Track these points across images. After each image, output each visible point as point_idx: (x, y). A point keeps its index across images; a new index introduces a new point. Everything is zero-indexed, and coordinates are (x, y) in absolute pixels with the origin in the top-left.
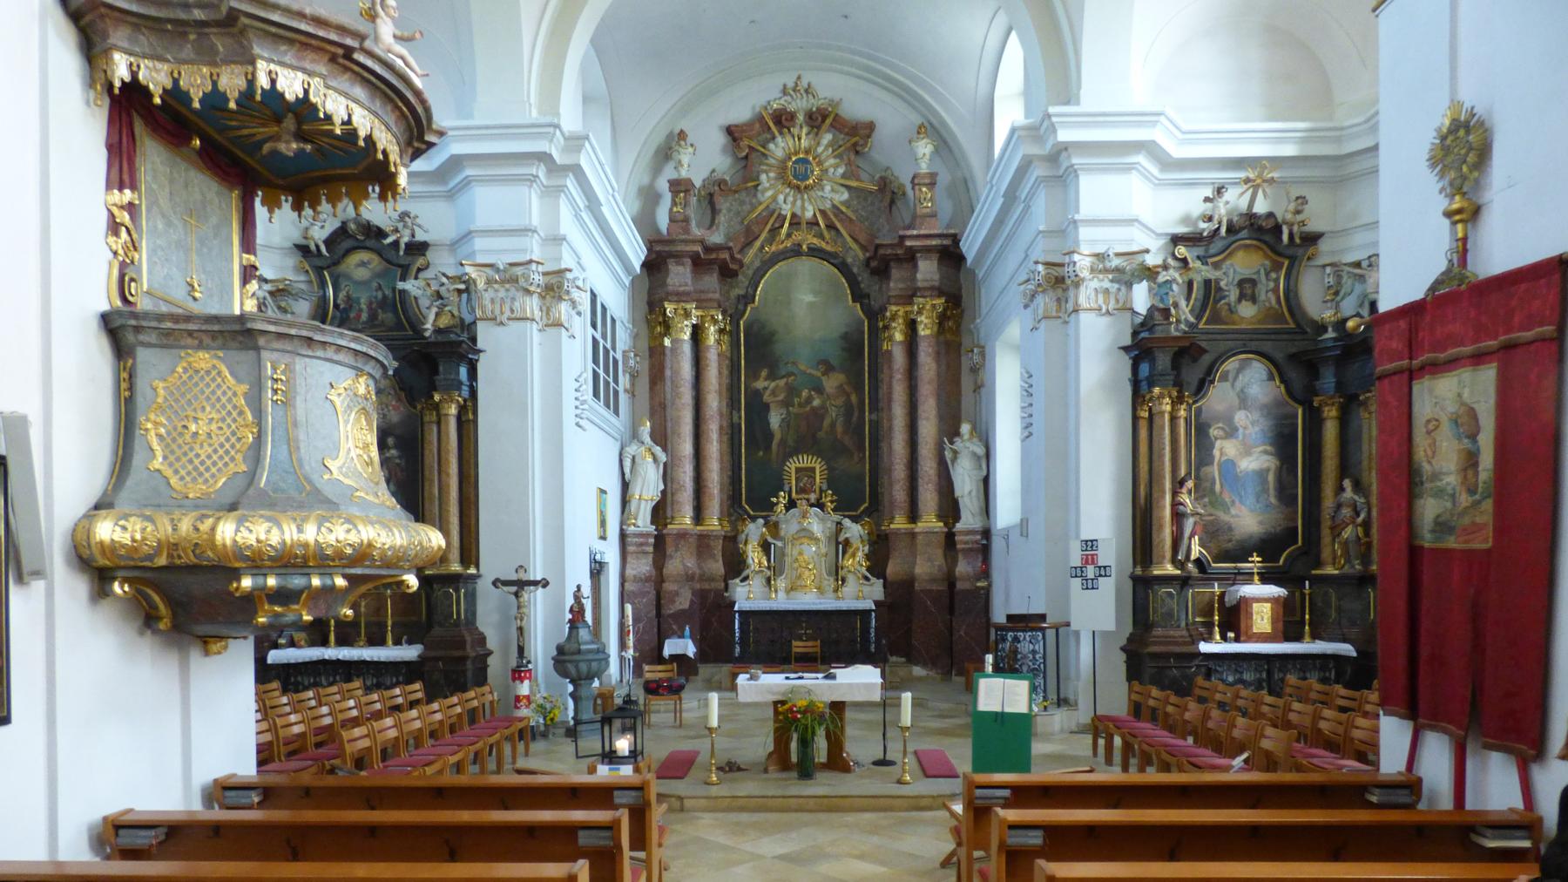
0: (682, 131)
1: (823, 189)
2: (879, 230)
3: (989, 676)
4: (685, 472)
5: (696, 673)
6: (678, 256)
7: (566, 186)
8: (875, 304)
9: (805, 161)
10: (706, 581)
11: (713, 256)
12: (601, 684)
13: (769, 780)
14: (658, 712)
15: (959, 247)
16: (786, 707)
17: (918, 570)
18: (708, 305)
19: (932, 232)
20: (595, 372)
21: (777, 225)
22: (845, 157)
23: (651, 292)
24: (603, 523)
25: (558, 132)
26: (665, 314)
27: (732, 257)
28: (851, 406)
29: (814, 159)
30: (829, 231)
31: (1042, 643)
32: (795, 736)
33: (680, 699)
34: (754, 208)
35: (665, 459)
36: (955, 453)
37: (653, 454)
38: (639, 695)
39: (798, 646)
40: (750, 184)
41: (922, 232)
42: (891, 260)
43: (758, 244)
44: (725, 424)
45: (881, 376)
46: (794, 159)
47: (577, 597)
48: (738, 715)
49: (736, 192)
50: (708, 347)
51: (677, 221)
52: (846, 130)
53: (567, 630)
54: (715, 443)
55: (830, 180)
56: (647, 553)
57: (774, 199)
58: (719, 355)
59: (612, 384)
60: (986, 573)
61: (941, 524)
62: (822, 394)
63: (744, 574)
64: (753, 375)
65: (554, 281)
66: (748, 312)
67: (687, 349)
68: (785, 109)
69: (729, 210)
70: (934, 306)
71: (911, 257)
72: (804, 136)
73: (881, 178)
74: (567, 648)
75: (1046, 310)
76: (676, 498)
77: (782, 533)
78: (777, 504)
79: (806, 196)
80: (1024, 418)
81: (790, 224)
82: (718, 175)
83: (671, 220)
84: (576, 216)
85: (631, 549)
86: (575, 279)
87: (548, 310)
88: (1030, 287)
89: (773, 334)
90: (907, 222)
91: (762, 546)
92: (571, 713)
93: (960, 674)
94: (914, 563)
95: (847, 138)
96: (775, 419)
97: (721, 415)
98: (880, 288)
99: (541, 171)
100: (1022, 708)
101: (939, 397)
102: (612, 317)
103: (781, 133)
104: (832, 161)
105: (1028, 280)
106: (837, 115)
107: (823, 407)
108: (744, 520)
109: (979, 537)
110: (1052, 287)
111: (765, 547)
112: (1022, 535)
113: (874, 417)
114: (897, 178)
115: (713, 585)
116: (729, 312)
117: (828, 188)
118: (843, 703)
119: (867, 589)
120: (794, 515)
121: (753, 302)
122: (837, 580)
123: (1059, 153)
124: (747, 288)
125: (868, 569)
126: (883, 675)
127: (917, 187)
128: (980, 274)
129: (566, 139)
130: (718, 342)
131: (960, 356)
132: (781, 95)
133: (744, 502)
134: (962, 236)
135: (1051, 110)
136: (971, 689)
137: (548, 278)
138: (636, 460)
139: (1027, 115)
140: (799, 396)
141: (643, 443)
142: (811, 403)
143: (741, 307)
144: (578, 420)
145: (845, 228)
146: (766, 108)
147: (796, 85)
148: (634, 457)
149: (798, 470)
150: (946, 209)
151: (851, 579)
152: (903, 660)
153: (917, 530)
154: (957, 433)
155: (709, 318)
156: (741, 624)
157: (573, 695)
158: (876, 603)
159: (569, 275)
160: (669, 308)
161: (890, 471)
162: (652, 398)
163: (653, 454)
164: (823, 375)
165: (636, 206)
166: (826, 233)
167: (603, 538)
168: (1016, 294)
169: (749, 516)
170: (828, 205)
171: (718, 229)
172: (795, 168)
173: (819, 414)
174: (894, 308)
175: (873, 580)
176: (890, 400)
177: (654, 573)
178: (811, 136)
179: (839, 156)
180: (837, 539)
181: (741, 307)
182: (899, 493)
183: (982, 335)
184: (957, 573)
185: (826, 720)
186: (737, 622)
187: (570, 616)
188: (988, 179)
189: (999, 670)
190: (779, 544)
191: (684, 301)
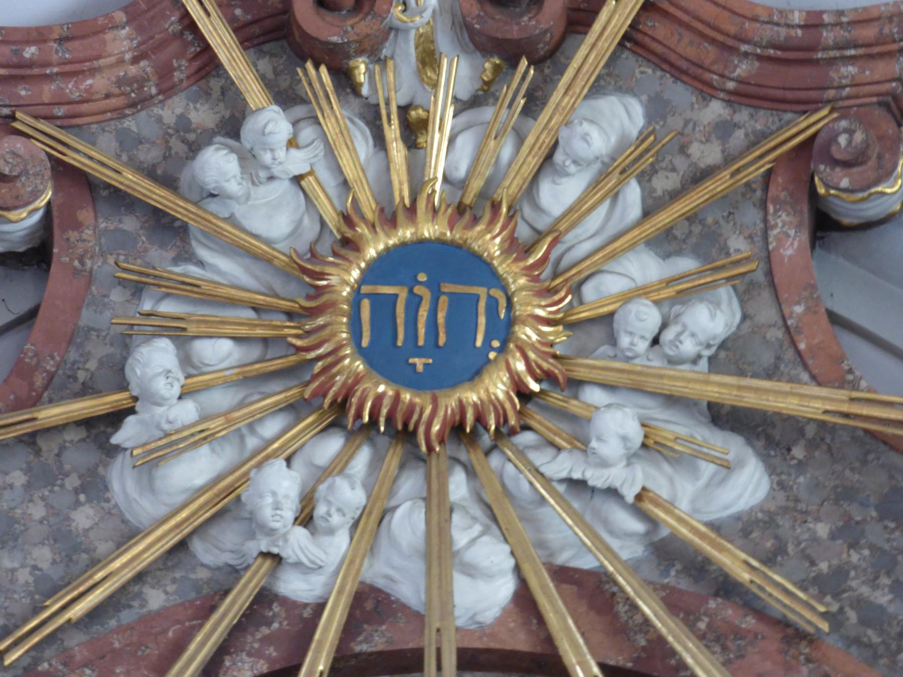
95: (763, 120)
161: (241, 297)
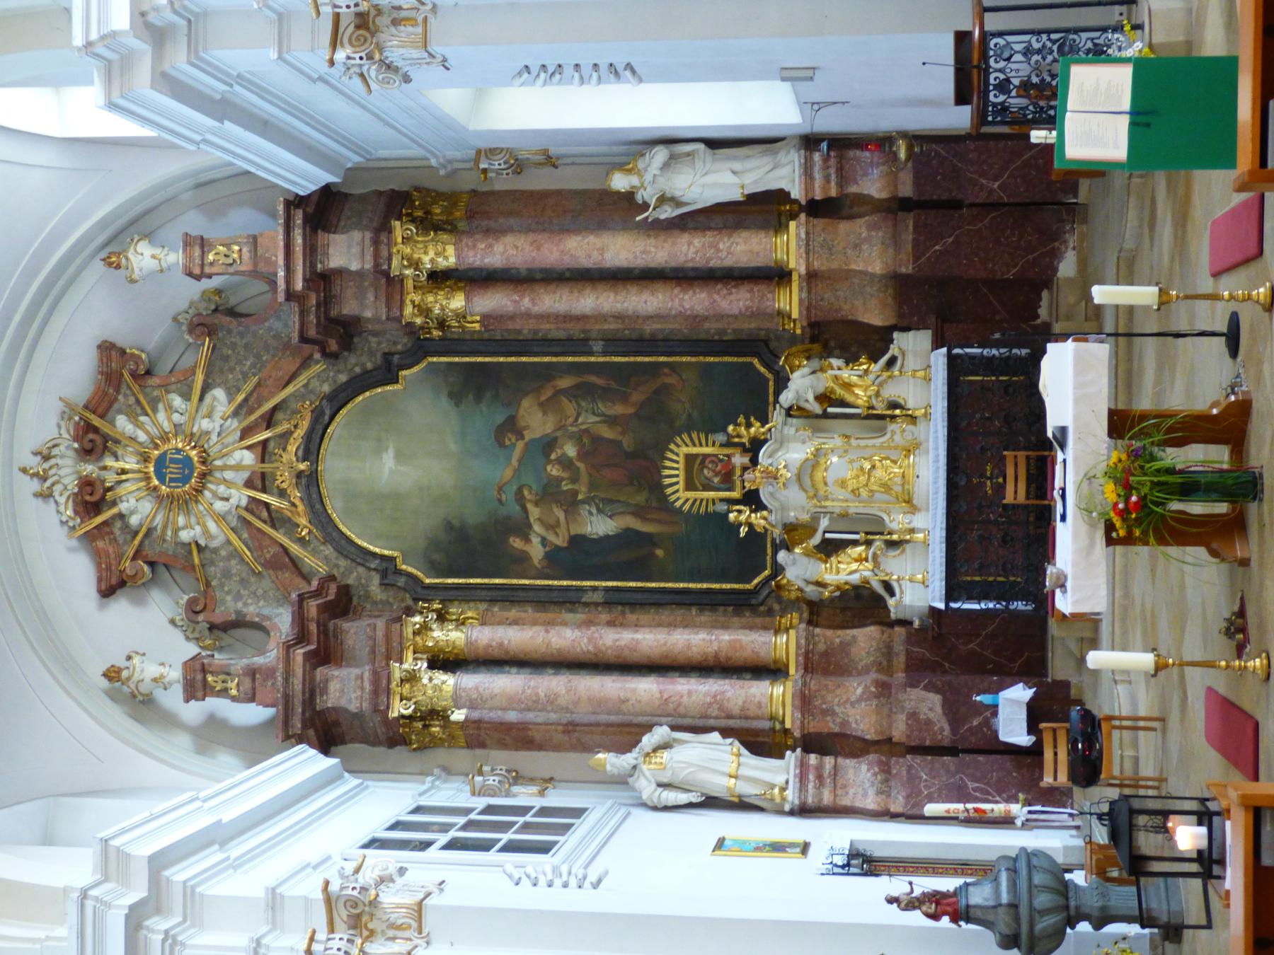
0: (105, 675)
1: (208, 433)
2: (277, 336)
3: (1061, 136)
4: (690, 693)
5: (1066, 685)
6: (312, 691)
7: (185, 882)
8: (403, 343)
9: (161, 463)
10: (890, 661)
11: (313, 627)
12: (1082, 867)
13: (1261, 558)
14: (1136, 760)
15: (309, 196)
16: (1118, 522)
17: (877, 267)
18: (396, 639)
19: (282, 244)
20: (506, 849)
21: (265, 514)
22: (155, 393)
23: (374, 742)
24: (778, 848)
25: (93, 893)
26: (410, 717)
27: (317, 594)
28: (577, 387)
29: (156, 447)
30: (276, 424)
31: (1010, 38)
32: (1175, 506)
33: (1110, 718)
34: (235, 554)
35: (665, 729)
36: (663, 200)
37: (655, 750)
38: (1103, 795)
39: (1016, 492)
40: (196, 561)
41: (281, 261)
42: (327, 318)
43: (295, 549)
44: (605, 617)
45: (526, 334)
46: (156, 482)
47: (910, 904)
48: (1143, 611)
49: (208, 584)
50: (469, 643)
51: (254, 689)
52: (111, 391)
53: (971, 926)
54: (639, 636)
55: (193, 420)
56: (835, 766)
57: (221, 518)
58: (483, 624)
59: (528, 818)
60: (881, 143)
61: (792, 224)
62: (555, 440)
63: (880, 589)
64: (520, 563)
65: (344, 914)
66: (410, 569)
67: (470, 681)
68: (75, 494)
69: (238, 597)
70: (406, 240)
71: (323, 281)
72: (121, 464)
73: (191, 331)
74: (1004, 927)
75: (413, 45)
76: (736, 711)
77: (805, 517)
78: (750, 525)
79: (218, 463)
80: (599, 80)
81: (264, 490)
82: (179, 614)
83: (252, 699)
84: (235, 868)
85: (827, 798)
86: (343, 876)
87: (393, 926)
88: (373, 73)
89: (449, 526)
90: (266, 287)
91: (828, 555)
92: (1134, 929)
93: (1074, 190)
94: (864, 273)
95: (124, 389)
96: (599, 526)
97: (589, 623)
98: (374, 334)
99: (157, 925)
100: (1126, 73)
101: (566, 231)
102: (413, 812)
103: (114, 503)
104: (161, 416)
105: (362, 75)
106: (86, 407)
107: (578, 438)
108: (779, 587)
109: (817, 157)
110: (373, 35)
111: (829, 549)
112: (811, 79)
113: (598, 347)
114: (192, 304)
115: (899, 648)
116: (410, 602)
117: (205, 424)
118: (1112, 413)
119: (911, 363)
120: (772, 494)
121: (392, 559)
122: (893, 417)
123: (148, 26)
124: (369, 569)
125: (874, 359)
126: (1063, 337)
127: (207, 270)
128: (354, 159)
129: (106, 879)
130: (461, 623)
131: (493, 193)
132: (52, 500)
133: (748, 586)
134: (289, 191)
135: (78, 41)
136: (1097, 171)
137: (339, 924)
138: (665, 780)
139: (87, 81)
140: (559, 480)
141: (635, 767)
142: (570, 460)
143: (401, 581)
144: (587, 884)
145: (272, 395)
146: (73, 528)
147: (36, 475)
148: (660, 785)
149: (690, 486)
150: (245, 220)
151: (892, 391)
152: (1045, 294)
153: (803, 270)
154: (629, 196)
155: (418, 639)
156: (970, 598)
157: (1099, 924)
158: (936, 345)
159: (334, 887)
160: (399, 709)
162: (557, 748)
163: (655, 750)
164: (522, 437)
165: (226, 759)
166: (279, 429)
167: (805, 848)
168: (387, 97)
169: (774, 576)
170: (234, 425)
171: (269, 618)
172: (171, 480)
173: (593, 447)
174: (409, 310)
175: (893, 350)
176: (568, 318)
177: (872, 757)
178: (120, 453)
179: (154, 403)
180: (817, 416)
181: (401, 581)
182: (735, 301)
183: (457, 155)
184: (884, 195)
185: (1144, 447)
186: (967, 606)
187: (946, 919)
188: (192, 148)
189: (1051, 121)
190: (824, 523)
191: (389, 682)
